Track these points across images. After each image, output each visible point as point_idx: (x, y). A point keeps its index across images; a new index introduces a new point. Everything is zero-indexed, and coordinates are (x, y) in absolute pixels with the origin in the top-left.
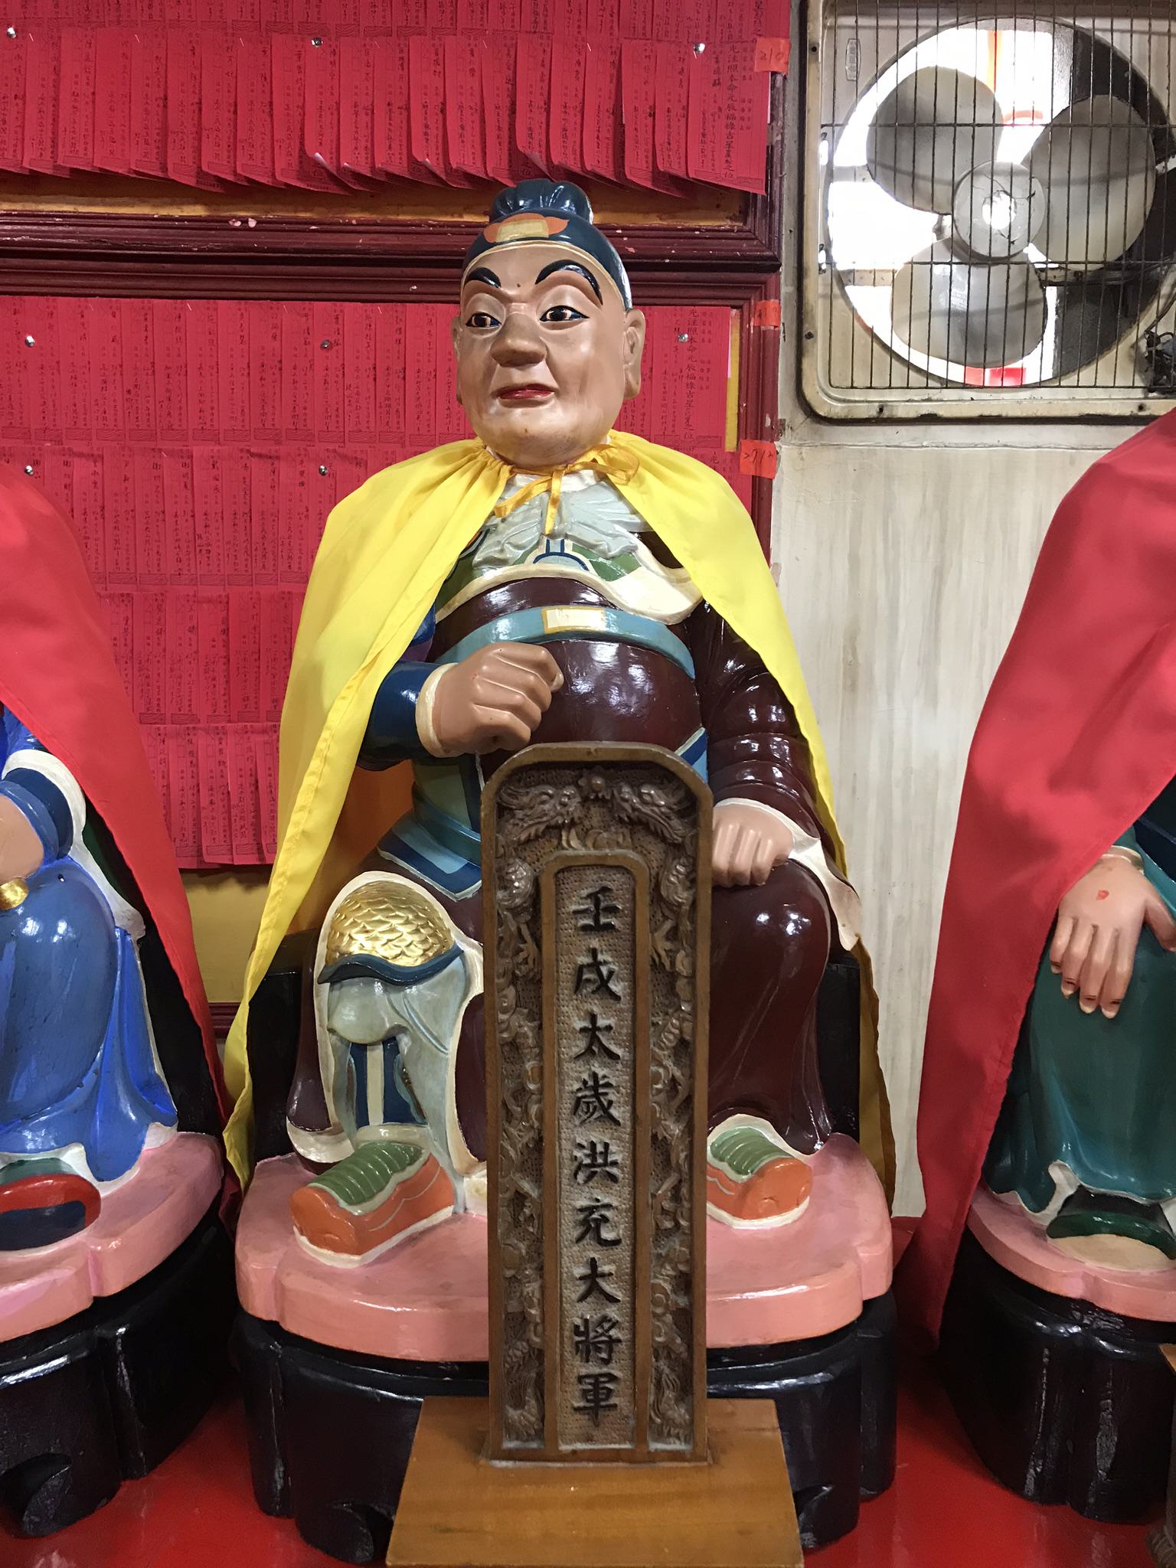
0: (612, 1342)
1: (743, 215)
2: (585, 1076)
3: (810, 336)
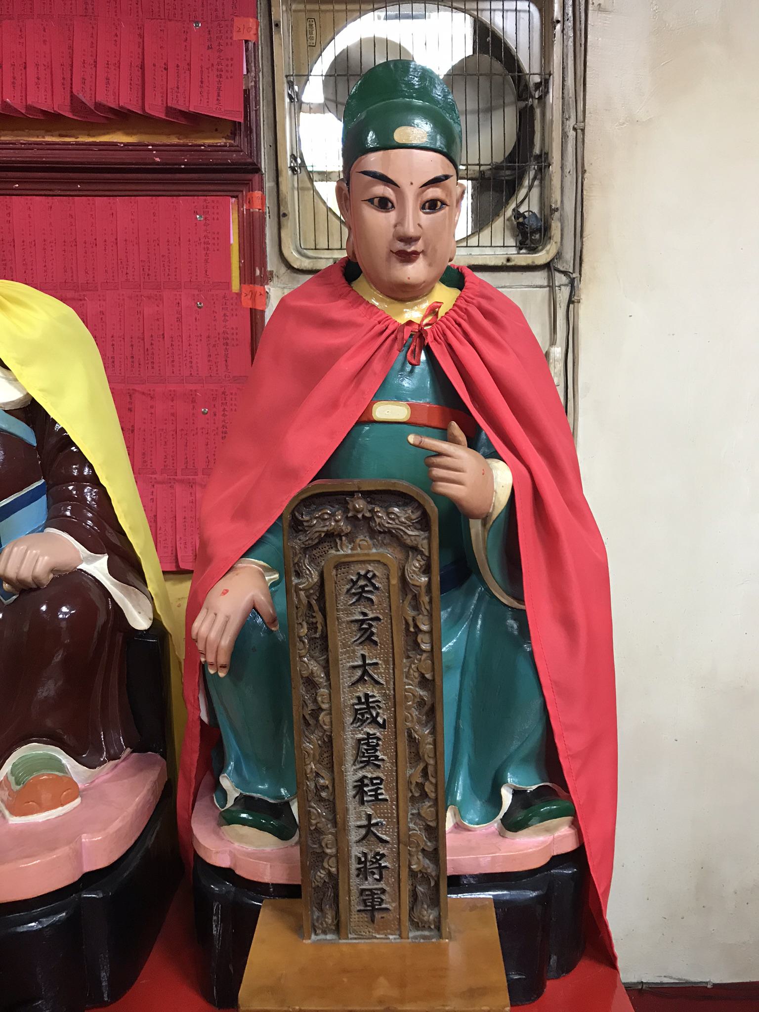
0: (381, 868)
1: (233, 135)
2: (361, 695)
3: (285, 215)
